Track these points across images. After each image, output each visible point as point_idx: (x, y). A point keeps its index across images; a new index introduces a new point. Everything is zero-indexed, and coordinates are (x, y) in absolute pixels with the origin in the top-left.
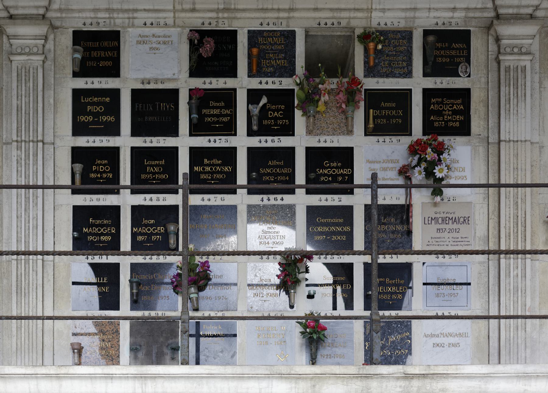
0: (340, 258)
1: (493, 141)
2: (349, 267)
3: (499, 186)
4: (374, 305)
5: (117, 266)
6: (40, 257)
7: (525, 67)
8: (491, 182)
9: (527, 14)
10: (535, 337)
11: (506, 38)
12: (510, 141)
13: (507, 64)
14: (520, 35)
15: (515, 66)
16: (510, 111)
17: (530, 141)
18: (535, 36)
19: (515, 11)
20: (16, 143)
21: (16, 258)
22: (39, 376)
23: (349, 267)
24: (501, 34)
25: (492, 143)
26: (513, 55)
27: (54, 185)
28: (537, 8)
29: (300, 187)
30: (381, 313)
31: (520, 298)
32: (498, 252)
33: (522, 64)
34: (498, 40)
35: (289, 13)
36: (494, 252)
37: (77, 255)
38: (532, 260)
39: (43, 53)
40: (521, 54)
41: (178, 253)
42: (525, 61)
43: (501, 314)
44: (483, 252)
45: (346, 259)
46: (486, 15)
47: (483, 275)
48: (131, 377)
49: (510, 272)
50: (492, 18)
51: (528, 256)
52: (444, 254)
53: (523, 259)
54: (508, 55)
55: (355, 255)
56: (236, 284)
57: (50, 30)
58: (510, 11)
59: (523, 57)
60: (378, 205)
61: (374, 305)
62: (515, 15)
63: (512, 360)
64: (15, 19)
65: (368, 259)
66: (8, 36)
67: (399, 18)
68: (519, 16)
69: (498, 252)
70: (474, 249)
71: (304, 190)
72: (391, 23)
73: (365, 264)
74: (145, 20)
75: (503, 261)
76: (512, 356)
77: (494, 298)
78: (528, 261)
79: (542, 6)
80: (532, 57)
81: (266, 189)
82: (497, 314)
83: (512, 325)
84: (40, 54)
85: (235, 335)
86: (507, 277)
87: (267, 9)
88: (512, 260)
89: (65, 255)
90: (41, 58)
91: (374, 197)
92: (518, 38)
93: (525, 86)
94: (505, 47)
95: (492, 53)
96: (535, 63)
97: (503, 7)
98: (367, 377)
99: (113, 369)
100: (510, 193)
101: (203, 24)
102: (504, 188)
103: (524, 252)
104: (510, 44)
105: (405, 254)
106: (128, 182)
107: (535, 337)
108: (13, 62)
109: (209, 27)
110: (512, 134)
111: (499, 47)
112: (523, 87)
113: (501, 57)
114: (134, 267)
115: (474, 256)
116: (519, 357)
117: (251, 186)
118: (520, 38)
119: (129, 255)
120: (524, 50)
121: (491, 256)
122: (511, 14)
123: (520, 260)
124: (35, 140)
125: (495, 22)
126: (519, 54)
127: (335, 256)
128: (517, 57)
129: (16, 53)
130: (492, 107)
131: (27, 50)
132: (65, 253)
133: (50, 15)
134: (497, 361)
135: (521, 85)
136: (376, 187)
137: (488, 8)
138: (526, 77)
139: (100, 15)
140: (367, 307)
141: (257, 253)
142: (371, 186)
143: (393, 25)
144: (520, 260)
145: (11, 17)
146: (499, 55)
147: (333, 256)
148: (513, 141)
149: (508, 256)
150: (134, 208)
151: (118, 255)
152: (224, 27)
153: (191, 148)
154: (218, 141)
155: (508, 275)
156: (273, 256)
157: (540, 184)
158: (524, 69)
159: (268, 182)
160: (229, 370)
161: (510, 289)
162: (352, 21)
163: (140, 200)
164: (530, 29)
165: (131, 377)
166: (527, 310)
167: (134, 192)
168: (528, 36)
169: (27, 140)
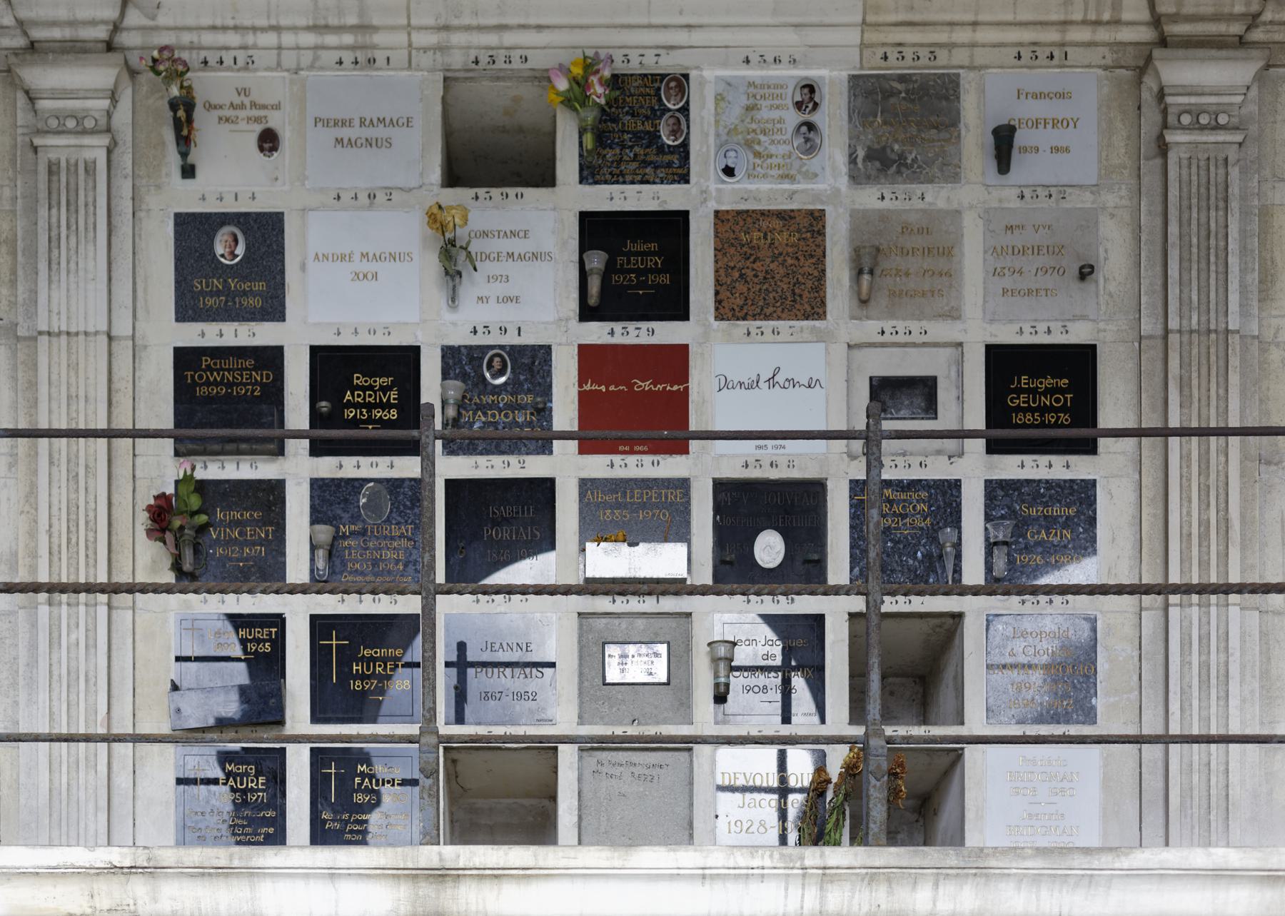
0: (628, 601)
1: (27, 334)
3: (1165, 433)
4: (874, 708)
5: (819, 619)
6: (103, 598)
7: (95, 162)
10: (123, 785)
11: (45, 96)
13: (53, 156)
14: (78, 90)
15: (72, 161)
16: (59, 263)
18: (1248, 88)
19: (67, 33)
20: (1178, 335)
21: (1179, 602)
24: (33, 87)
25: (1150, 337)
26: (62, 136)
27: (1140, 436)
28: (1253, 20)
29: (298, 435)
30: (889, 731)
33: (88, 155)
37: (318, 592)
39: (108, 130)
40: (85, 132)
42: (95, 148)
43: (1171, 732)
44: (1120, 590)
45: (805, 605)
46: (1126, 35)
47: (7, 641)
51: (1233, 598)
53: (91, 605)
54: (51, 136)
56: (553, 665)
57: (126, 76)
58: (56, 33)
59: (87, 140)
61: (874, 708)
62: (71, 44)
63: (1214, 838)
64: (46, 52)
65: (857, 603)
66: (27, 92)
67: (658, 47)
68: (78, 45)
70: (1071, 583)
71: (306, 443)
72: (623, 58)
73: (852, 616)
75: (1174, 613)
77: (30, 695)
78: (1234, 612)
79: (1267, 16)
81: (340, 441)
82: (1159, 731)
84: (100, 132)
85: (180, 781)
87: (327, 27)
88: (64, 607)
89: (21, 591)
90: (104, 140)
91: (874, 462)
93: (95, 207)
94: (47, 115)
95: (25, 131)
96: (123, 153)
98: (441, 875)
99: (268, 857)
101: (886, 58)
102: (46, 440)
103: (1226, 589)
104: (59, 109)
105: (943, 594)
106: (304, 424)
108: (39, 149)
110: (64, 317)
111: (1165, 112)
112: (92, 208)
116: (82, 831)
118: (80, 96)
119: (304, 592)
121: (1147, 599)
122: (60, 41)
123: (82, 609)
124: (1203, 327)
125: (1157, 53)
127: (913, 598)
128: (72, 140)
129: (46, 129)
130: (24, 255)
131: (1204, 120)
132: (156, 589)
133: (126, 39)
134: (1162, 840)
135: (86, 205)
136: (431, 438)
137: (7, 27)
138: (95, 187)
139: (288, 39)
140: (857, 711)
141: (299, 589)
142: (864, 435)
144: (1213, 610)
145: (32, 46)
146: (1165, 131)
147: (763, 597)
148: (68, 333)
149: (56, 596)
153: (582, 348)
154: (633, 333)
155: (54, 642)
157: (1272, 427)
158: (90, 169)
159: (355, 423)
160: (686, 858)
161: (60, 676)
162: (978, 51)
163: (599, 466)
164: (100, 75)
167: (587, 447)
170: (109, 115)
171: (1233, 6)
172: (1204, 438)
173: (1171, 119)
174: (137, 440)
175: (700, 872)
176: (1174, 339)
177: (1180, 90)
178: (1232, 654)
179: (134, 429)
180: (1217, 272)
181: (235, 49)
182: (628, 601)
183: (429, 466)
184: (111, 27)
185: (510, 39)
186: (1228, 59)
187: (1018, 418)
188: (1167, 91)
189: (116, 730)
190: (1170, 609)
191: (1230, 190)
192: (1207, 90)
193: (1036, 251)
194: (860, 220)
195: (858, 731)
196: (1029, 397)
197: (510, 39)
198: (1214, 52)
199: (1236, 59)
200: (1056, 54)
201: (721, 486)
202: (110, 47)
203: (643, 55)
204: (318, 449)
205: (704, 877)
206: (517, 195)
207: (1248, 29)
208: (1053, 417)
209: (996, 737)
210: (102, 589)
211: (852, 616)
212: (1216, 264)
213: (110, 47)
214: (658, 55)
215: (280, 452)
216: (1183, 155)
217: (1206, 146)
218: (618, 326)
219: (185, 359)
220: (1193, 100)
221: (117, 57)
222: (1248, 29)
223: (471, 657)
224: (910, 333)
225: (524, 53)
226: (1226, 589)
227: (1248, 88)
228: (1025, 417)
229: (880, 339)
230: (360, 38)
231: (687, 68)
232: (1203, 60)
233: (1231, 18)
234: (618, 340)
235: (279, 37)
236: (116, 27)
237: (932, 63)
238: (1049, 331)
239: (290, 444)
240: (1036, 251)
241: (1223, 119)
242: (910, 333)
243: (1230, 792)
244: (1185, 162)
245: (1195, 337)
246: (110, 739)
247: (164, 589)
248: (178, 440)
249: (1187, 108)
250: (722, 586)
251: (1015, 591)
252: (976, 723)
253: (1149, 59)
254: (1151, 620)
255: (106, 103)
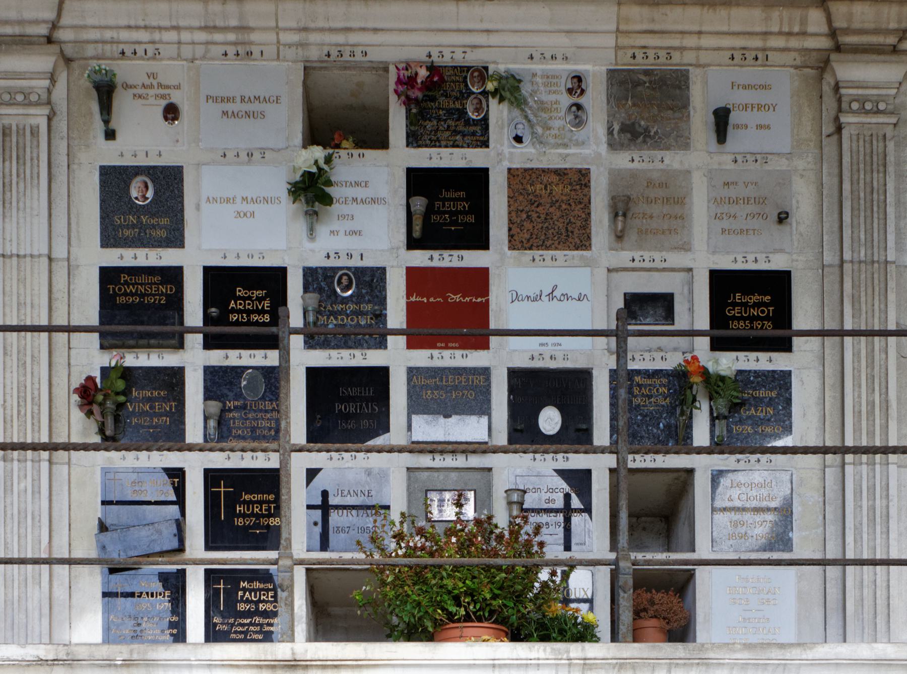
2: (586, 474)
3: (841, 333)
6: (45, 455)
7: (38, 127)
8: (63, 336)
9: (39, 36)
10: (62, 597)
12: (11, 256)
14: (24, 72)
15: (21, 127)
17: (894, 262)
18: (900, 83)
19: (17, 30)
22: (84, 662)
23: (586, 474)
25: (830, 266)
26: (13, 107)
29: (296, 331)
31: (29, 530)
32: (842, 450)
33: (33, 121)
34: (837, 88)
35: (787, 41)
36: (833, 450)
38: (898, 467)
41: (179, 445)
43: (847, 557)
44: (814, 450)
48: (268, 666)
49: (12, 485)
50: (826, 50)
51: (892, 458)
52: (120, 451)
53: (36, 461)
54: (5, 107)
55: (580, 453)
57: (61, 63)
59: (32, 111)
60: (628, 370)
62: (20, 38)
67: (465, 46)
68: (25, 38)
69: (842, 450)
74: (430, 49)
75: (849, 469)
76: (16, 630)
80: (896, 119)
83: (29, 575)
84: (43, 104)
86: (9, 492)
87: (215, 27)
92: (23, 77)
93: (38, 161)
97: (847, 31)
100: (12, 347)
103: (886, 450)
107: (62, 597)
109: (645, 65)
111: (839, 101)
113: (844, 119)
114: (212, 477)
115: (799, 457)
116: (29, 633)
117: (107, 328)
118: (26, 77)
119: (505, 452)
120: (868, 106)
121: (829, 457)
125: (834, 56)
126: (25, 105)
128: (21, 111)
131: (868, 106)
143: (443, 56)
146: (840, 114)
150: (412, 372)
151: (180, 450)
152: (645, 65)
154: (447, 259)
156: (239, 453)
158: (35, 131)
163: (422, 358)
165: (268, 666)
166: (42, 551)
168: (39, 73)
169: (856, 259)
170: (49, 92)
171: (889, 23)
172: (870, 338)
173: (845, 106)
174: (71, 333)
175: (582, 662)
176: (847, 267)
177: (850, 84)
178: (892, 500)
179: (69, 326)
180: (878, 218)
181: (146, 43)
182: (444, 459)
183: (285, 357)
184: (50, 26)
185: (353, 38)
186: (885, 62)
187: (234, 317)
188: (841, 84)
189: (56, 555)
190: (846, 466)
191: (888, 158)
192: (870, 84)
193: (746, 201)
194: (616, 176)
195: (612, 556)
196: (741, 309)
197: (353, 38)
198: (874, 57)
199: (891, 62)
200: (760, 56)
201: (513, 373)
202: (50, 40)
203: (454, 52)
204: (211, 343)
205: (494, 666)
206: (359, 155)
207: (900, 40)
208: (759, 324)
209: (714, 560)
210: (44, 447)
211: (611, 471)
212: (878, 212)
213: (50, 40)
214: (465, 52)
215: (485, 346)
216: (852, 132)
217: (870, 125)
218: (436, 254)
219: (108, 275)
220: (860, 92)
221: (54, 48)
222: (900, 40)
223: (333, 501)
224: (654, 260)
225: (364, 49)
226: (886, 450)
227: (900, 83)
228: (739, 324)
229: (631, 265)
230: (240, 37)
231: (487, 62)
232: (867, 62)
233: (888, 32)
234: (436, 263)
235: (179, 34)
236: (55, 26)
237: (669, 62)
238: (756, 261)
239: (189, 338)
240: (746, 201)
241: (882, 106)
242: (654, 260)
243: (891, 602)
244: (855, 138)
245: (863, 266)
246: (49, 561)
247: (802, 451)
248: (306, 336)
249: (856, 97)
250: (513, 447)
251: (728, 451)
252: (703, 550)
253: (827, 61)
254: (831, 474)
255: (46, 83)
